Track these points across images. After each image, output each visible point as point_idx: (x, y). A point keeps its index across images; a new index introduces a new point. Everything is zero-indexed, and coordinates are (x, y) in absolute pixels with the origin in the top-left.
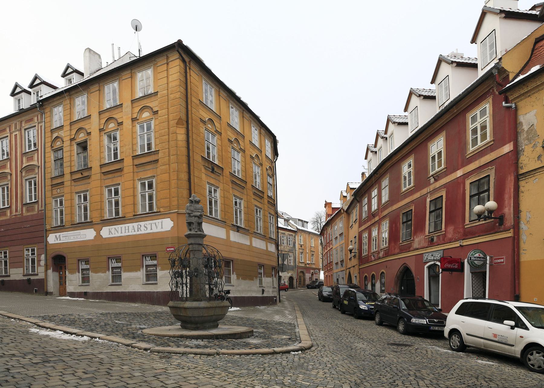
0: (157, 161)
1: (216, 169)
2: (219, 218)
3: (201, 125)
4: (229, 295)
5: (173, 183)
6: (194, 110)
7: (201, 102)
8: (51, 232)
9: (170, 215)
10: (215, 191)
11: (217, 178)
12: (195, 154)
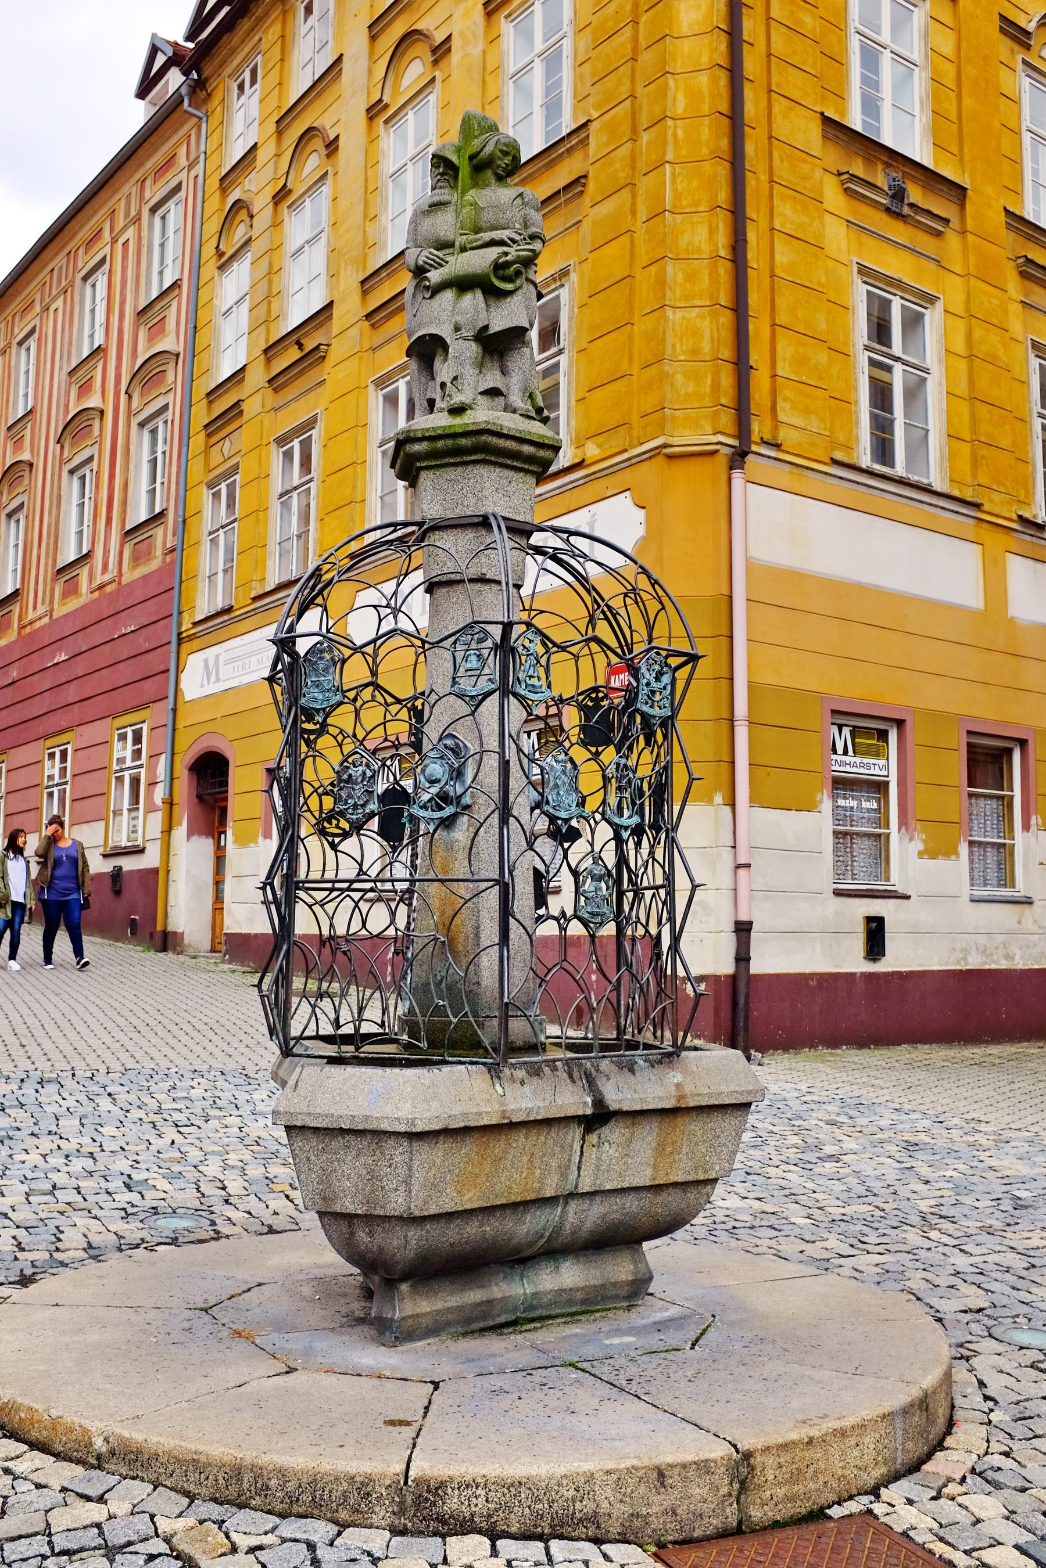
0: (579, 182)
1: (915, 194)
8: (196, 643)
9: (626, 477)
10: (913, 322)
12: (780, 106)
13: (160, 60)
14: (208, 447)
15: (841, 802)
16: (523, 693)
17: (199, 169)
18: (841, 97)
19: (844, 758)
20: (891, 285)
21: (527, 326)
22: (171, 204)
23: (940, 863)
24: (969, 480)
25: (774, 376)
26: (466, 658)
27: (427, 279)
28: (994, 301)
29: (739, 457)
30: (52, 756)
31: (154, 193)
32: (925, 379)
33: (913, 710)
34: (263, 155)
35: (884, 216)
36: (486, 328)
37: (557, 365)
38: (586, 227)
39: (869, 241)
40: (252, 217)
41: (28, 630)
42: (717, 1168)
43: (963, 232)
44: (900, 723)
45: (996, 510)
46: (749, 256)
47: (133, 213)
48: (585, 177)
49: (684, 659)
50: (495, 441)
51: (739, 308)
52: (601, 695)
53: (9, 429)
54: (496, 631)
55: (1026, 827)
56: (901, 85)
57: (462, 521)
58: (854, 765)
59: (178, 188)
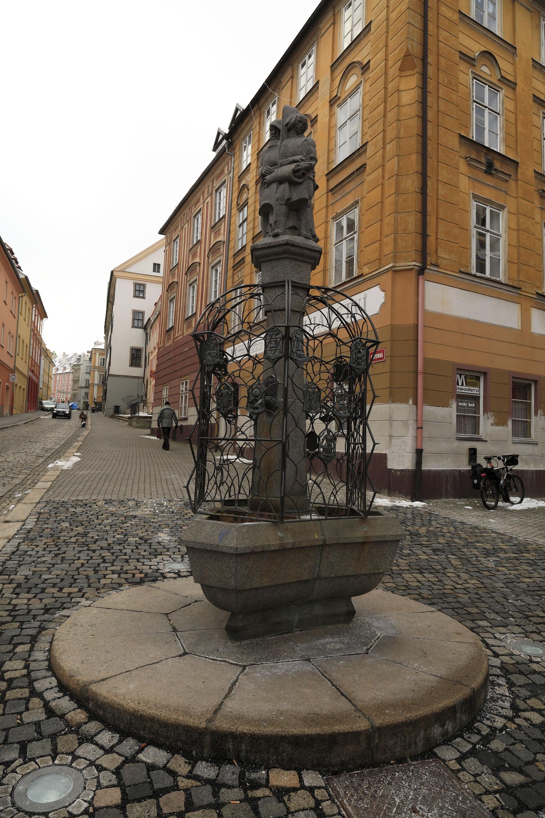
0: (364, 166)
1: (497, 165)
2: (502, 278)
3: (463, 66)
4: (516, 468)
5: (389, 207)
6: (443, 34)
7: (463, 16)
10: (495, 216)
11: (502, 185)
12: (442, 131)
13: (221, 137)
14: (233, 274)
15: (460, 404)
16: (295, 358)
17: (231, 175)
18: (467, 127)
19: (463, 387)
20: (486, 202)
21: (307, 197)
22: (222, 188)
23: (500, 428)
24: (516, 278)
25: (437, 239)
26: (270, 342)
27: (265, 179)
28: (529, 207)
29: (421, 271)
30: (183, 383)
31: (217, 185)
32: (499, 239)
33: (540, 377)
34: (253, 167)
35: (485, 175)
36: (289, 199)
37: (354, 238)
38: (365, 185)
39: (478, 185)
40: (248, 190)
41: (176, 340)
42: (384, 568)
43: (517, 180)
44: (485, 374)
45: (527, 290)
46: (428, 191)
47: (210, 192)
48: (365, 164)
49: (372, 343)
50: (292, 249)
51: (424, 212)
52: (343, 360)
53: (171, 270)
54: (283, 330)
55: (536, 414)
56: (493, 122)
57: (279, 284)
58: (463, 389)
59: (225, 182)
